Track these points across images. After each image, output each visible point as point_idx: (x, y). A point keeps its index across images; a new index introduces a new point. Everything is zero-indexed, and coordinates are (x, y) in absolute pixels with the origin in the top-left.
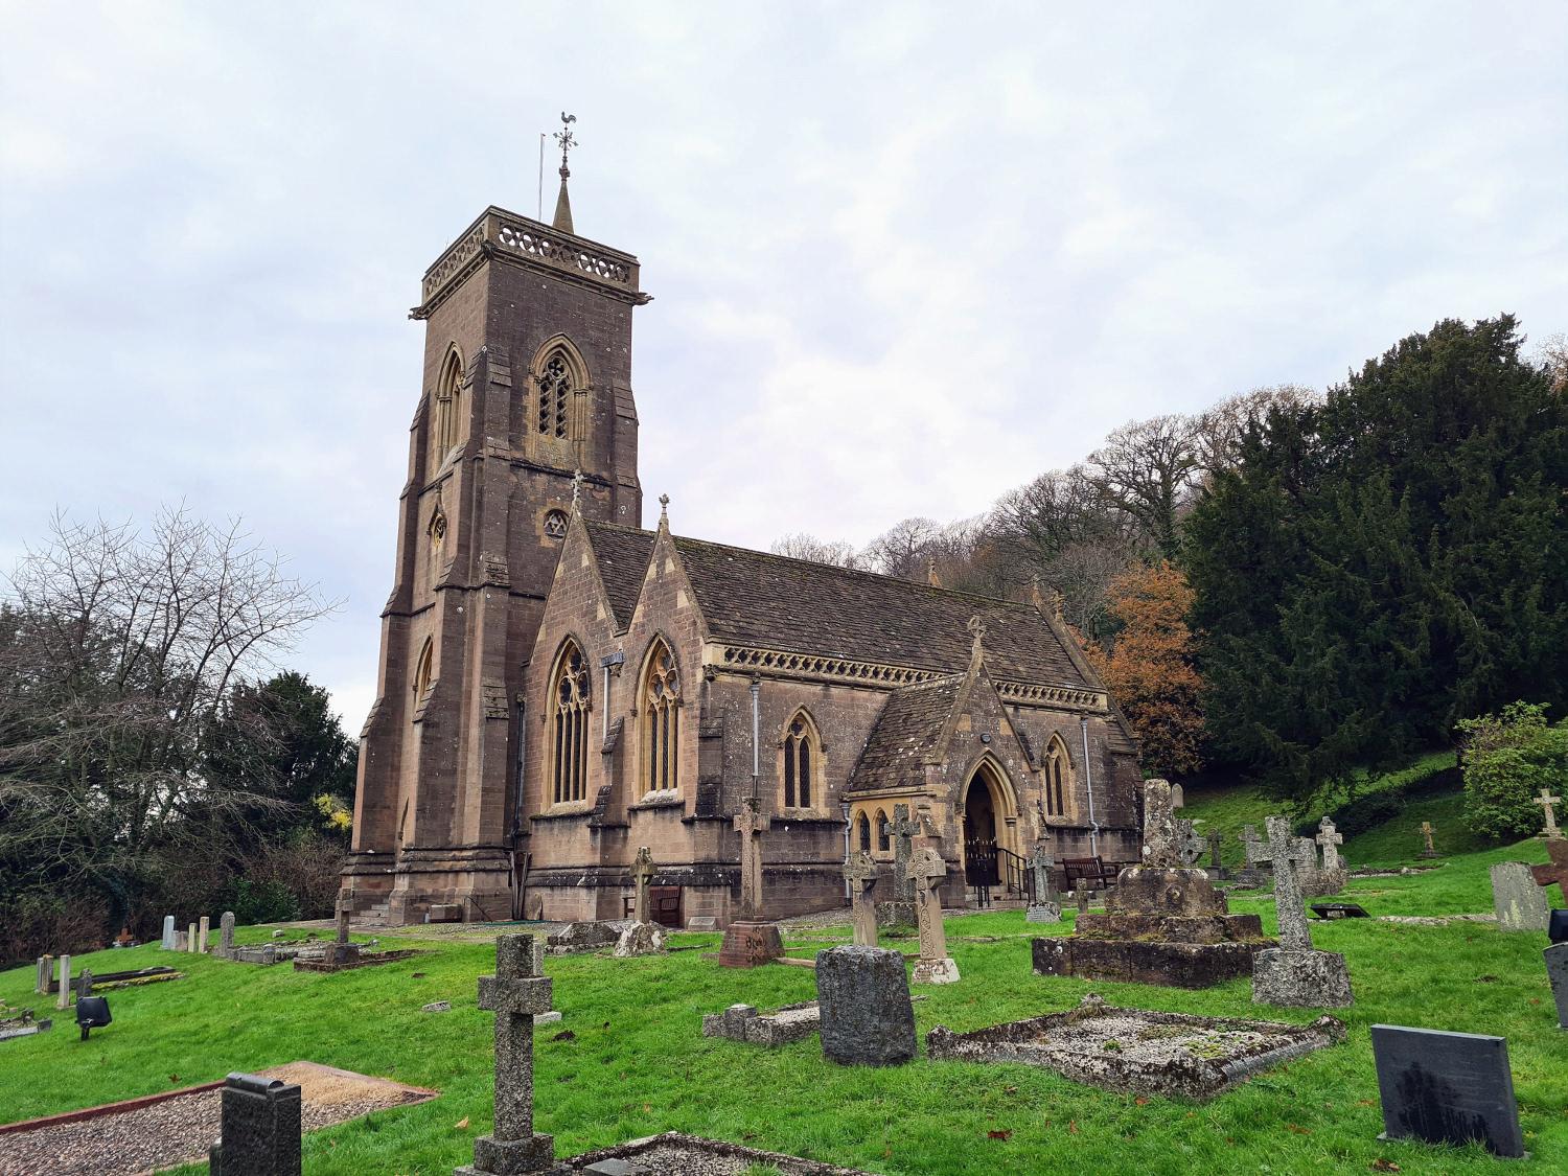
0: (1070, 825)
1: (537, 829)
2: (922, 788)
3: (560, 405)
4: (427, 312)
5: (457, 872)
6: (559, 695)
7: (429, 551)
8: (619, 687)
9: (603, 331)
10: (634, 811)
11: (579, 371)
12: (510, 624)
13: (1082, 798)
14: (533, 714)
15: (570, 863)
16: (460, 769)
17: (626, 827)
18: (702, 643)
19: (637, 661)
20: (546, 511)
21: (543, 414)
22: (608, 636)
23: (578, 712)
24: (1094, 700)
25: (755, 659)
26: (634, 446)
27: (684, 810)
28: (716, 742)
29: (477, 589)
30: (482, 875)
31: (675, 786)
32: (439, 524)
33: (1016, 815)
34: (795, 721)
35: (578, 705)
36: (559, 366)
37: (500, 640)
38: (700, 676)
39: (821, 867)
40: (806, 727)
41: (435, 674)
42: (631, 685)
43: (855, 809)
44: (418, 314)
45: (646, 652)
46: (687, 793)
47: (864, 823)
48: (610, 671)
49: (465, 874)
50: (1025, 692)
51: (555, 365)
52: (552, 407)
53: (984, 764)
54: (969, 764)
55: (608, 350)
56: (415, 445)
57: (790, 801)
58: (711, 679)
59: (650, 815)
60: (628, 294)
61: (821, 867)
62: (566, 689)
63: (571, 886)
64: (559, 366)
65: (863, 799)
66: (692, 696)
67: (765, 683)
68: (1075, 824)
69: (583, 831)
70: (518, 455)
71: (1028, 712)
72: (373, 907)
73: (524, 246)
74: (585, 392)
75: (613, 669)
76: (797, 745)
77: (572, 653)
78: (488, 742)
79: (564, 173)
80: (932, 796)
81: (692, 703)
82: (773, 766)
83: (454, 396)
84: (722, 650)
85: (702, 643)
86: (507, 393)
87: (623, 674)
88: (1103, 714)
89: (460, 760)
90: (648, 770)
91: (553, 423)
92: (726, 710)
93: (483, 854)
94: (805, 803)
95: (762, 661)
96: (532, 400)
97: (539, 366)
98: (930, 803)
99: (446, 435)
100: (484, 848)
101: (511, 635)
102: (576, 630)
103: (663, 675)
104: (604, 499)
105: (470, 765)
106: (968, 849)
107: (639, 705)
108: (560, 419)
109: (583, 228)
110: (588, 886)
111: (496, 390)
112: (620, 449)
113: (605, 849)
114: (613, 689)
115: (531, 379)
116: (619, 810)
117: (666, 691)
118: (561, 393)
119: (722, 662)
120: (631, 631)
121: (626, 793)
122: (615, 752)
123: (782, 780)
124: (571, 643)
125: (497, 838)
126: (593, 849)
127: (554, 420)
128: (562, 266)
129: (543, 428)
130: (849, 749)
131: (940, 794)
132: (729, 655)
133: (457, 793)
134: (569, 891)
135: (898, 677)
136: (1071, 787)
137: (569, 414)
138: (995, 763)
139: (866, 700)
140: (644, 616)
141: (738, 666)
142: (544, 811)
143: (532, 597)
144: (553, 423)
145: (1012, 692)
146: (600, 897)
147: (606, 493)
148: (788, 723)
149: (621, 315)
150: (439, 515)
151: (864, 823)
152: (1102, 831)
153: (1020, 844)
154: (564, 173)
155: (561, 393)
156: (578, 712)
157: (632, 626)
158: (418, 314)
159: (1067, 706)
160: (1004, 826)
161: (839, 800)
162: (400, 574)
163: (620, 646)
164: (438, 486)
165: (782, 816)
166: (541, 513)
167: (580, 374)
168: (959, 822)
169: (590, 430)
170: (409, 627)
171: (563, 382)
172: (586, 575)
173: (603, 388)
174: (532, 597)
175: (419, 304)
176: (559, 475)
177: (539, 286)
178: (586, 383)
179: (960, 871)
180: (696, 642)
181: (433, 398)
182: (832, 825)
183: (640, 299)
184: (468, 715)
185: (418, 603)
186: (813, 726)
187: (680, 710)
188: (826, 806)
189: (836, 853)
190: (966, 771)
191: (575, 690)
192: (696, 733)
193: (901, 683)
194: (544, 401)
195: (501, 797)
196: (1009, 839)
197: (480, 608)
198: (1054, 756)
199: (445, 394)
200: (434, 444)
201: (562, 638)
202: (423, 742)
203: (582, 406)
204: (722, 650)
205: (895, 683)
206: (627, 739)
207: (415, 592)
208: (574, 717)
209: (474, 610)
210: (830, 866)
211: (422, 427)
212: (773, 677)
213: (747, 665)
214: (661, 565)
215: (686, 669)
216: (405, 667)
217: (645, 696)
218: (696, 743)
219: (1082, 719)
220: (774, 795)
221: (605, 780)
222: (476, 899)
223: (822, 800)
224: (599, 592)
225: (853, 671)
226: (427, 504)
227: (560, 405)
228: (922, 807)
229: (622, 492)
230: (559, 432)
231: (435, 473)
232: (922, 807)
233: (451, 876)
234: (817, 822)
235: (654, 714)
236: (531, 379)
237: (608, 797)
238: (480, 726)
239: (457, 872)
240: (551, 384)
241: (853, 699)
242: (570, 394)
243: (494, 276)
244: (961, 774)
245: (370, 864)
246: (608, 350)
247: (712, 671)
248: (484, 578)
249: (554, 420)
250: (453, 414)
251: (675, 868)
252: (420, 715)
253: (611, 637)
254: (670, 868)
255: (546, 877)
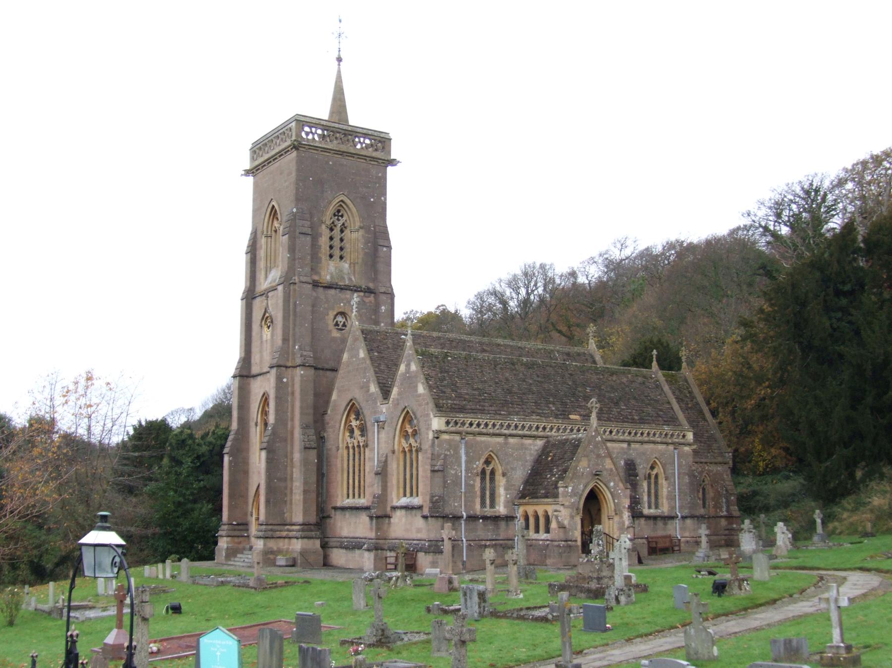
0: (663, 515)
1: (335, 515)
2: (557, 500)
3: (342, 240)
4: (253, 173)
5: (290, 538)
6: (348, 434)
7: (261, 337)
8: (383, 435)
9: (368, 187)
10: (394, 508)
11: (353, 217)
12: (315, 388)
13: (671, 498)
14: (330, 444)
15: (357, 535)
16: (289, 477)
17: (389, 517)
18: (432, 416)
19: (395, 421)
20: (335, 313)
21: (331, 247)
22: (377, 403)
23: (359, 446)
24: (684, 436)
25: (463, 424)
26: (389, 264)
27: (422, 510)
28: (440, 474)
29: (295, 367)
30: (306, 540)
31: (417, 496)
32: (267, 319)
33: (613, 514)
34: (487, 459)
35: (359, 442)
36: (340, 214)
37: (310, 399)
38: (431, 436)
39: (501, 542)
40: (493, 463)
41: (271, 419)
42: (391, 435)
43: (521, 510)
44: (248, 173)
45: (400, 416)
46: (424, 501)
47: (527, 518)
48: (378, 425)
49: (295, 540)
50: (636, 434)
51: (338, 214)
52: (336, 243)
53: (595, 486)
54: (585, 487)
55: (372, 200)
56: (249, 264)
57: (483, 504)
58: (437, 438)
59: (403, 512)
60: (384, 160)
61: (501, 542)
62: (352, 431)
63: (358, 549)
64: (340, 214)
65: (526, 504)
66: (426, 446)
67: (470, 437)
68: (666, 514)
69: (364, 518)
70: (316, 278)
71: (637, 446)
72: (239, 555)
73: (312, 136)
74: (358, 231)
75: (381, 425)
76: (488, 473)
77: (354, 409)
78: (305, 462)
79: (339, 60)
80: (563, 505)
81: (426, 450)
82: (473, 486)
83: (273, 233)
84: (444, 420)
85: (432, 416)
86: (309, 239)
87: (386, 427)
88: (689, 445)
89: (289, 472)
90: (402, 485)
91: (337, 253)
92: (446, 455)
93: (306, 527)
94: (493, 505)
95: (467, 425)
96: (324, 241)
97: (328, 218)
98: (561, 508)
99: (269, 259)
100: (306, 525)
101: (316, 395)
102: (357, 396)
103: (410, 431)
104: (370, 302)
105: (295, 476)
106: (583, 533)
107: (396, 447)
108: (341, 249)
109: (356, 118)
110: (368, 550)
111: (303, 238)
112: (381, 267)
113: (378, 529)
114: (380, 436)
115: (324, 227)
116: (386, 507)
117: (412, 441)
118: (342, 231)
119: (443, 427)
120: (390, 402)
121: (389, 499)
122: (382, 473)
123: (479, 493)
124: (354, 404)
125: (313, 519)
126: (371, 529)
127: (338, 251)
128: (343, 148)
129: (331, 256)
130: (520, 474)
131: (567, 504)
132: (448, 423)
133: (288, 492)
134: (357, 552)
135: (551, 429)
136: (664, 491)
137: (348, 246)
138: (602, 484)
139: (530, 445)
140: (398, 394)
141: (454, 429)
142: (339, 504)
143: (327, 370)
144: (337, 253)
145: (626, 434)
146: (376, 556)
147: (372, 298)
148: (482, 460)
149: (380, 175)
150: (267, 315)
151: (527, 518)
152: (684, 518)
153: (615, 530)
154: (339, 60)
155: (342, 231)
156: (359, 446)
157: (391, 400)
158: (248, 173)
159: (664, 440)
160: (607, 519)
161: (512, 504)
162: (243, 350)
163: (384, 411)
164: (265, 294)
165: (478, 513)
166: (331, 314)
167: (353, 218)
168: (578, 520)
169: (361, 256)
170: (249, 384)
171: (343, 224)
172: (362, 363)
173: (370, 227)
174: (327, 370)
175: (248, 167)
176: (342, 289)
177: (327, 163)
178: (358, 224)
179: (577, 546)
180: (428, 415)
181: (259, 233)
182: (510, 518)
183: (393, 162)
184: (292, 445)
185: (255, 370)
186: (497, 461)
187: (420, 455)
188: (505, 507)
189: (510, 533)
190: (583, 491)
191: (357, 433)
192: (428, 467)
193: (553, 433)
194: (331, 238)
195: (314, 496)
196: (609, 527)
197: (297, 380)
198: (654, 472)
199: (267, 232)
200: (261, 264)
201: (349, 400)
202: (267, 462)
203: (355, 238)
204: (444, 420)
205: (549, 433)
206: (389, 467)
207: (253, 361)
208: (356, 449)
209: (293, 380)
210: (506, 542)
211: (253, 250)
212: (474, 434)
213: (458, 428)
214: (408, 365)
215: (423, 430)
216: (248, 409)
217: (400, 442)
218: (429, 474)
219: (675, 449)
220: (474, 502)
221: (377, 490)
222: (303, 553)
223: (502, 505)
224: (371, 374)
225: (523, 427)
226: (258, 305)
227: (342, 240)
228: (556, 511)
229: (383, 298)
230: (341, 258)
231: (263, 284)
232: (556, 511)
233: (286, 540)
234: (499, 517)
235: (404, 452)
236: (324, 227)
237: (382, 499)
238: (301, 452)
239: (290, 538)
240: (335, 226)
241: (522, 444)
242: (347, 232)
243: (300, 161)
244: (580, 492)
245: (235, 530)
246: (372, 200)
247: (438, 434)
248: (298, 361)
249: (338, 251)
250: (357, 460)
251: (418, 542)
252: (265, 445)
253: (379, 404)
254: (415, 542)
255: (342, 543)
